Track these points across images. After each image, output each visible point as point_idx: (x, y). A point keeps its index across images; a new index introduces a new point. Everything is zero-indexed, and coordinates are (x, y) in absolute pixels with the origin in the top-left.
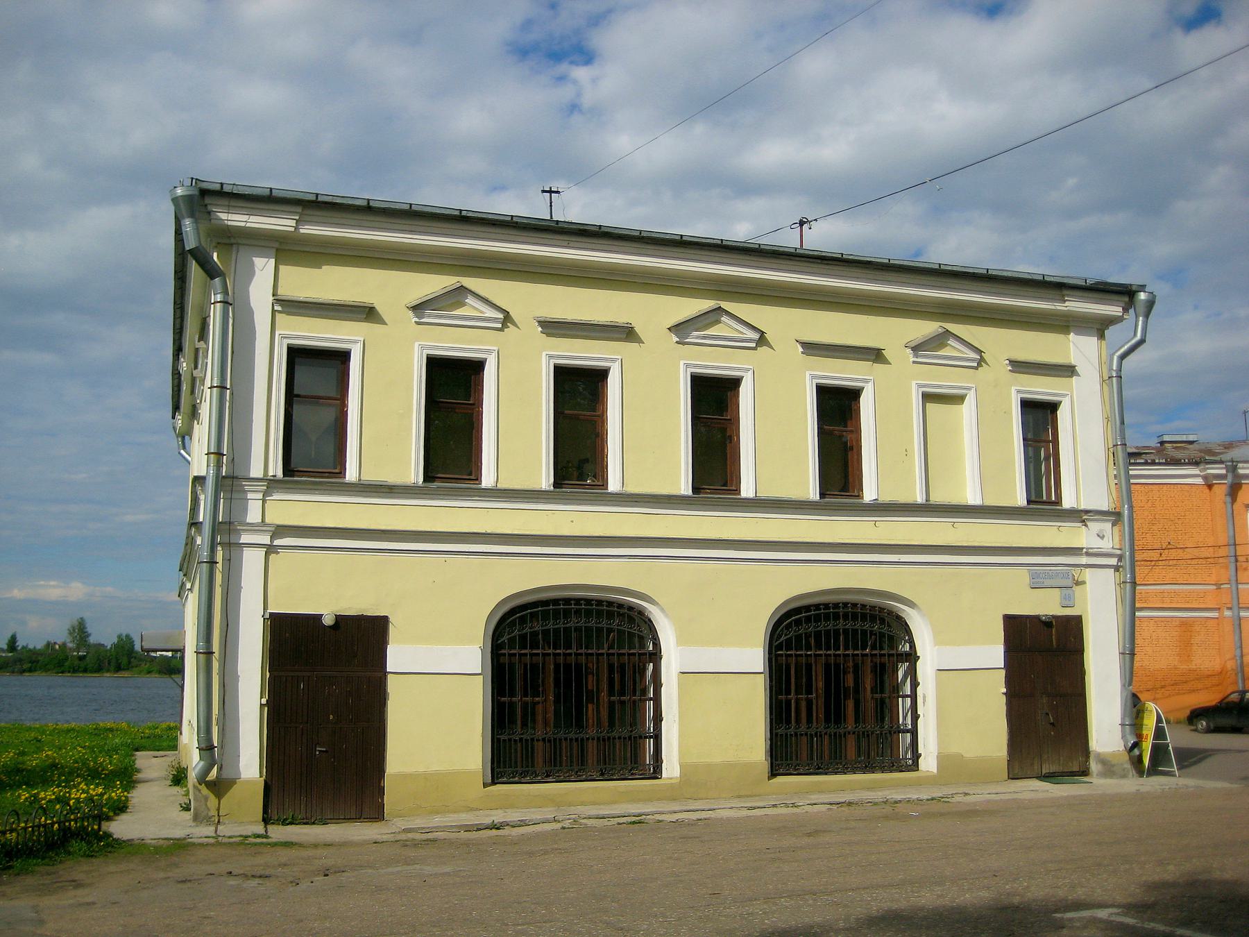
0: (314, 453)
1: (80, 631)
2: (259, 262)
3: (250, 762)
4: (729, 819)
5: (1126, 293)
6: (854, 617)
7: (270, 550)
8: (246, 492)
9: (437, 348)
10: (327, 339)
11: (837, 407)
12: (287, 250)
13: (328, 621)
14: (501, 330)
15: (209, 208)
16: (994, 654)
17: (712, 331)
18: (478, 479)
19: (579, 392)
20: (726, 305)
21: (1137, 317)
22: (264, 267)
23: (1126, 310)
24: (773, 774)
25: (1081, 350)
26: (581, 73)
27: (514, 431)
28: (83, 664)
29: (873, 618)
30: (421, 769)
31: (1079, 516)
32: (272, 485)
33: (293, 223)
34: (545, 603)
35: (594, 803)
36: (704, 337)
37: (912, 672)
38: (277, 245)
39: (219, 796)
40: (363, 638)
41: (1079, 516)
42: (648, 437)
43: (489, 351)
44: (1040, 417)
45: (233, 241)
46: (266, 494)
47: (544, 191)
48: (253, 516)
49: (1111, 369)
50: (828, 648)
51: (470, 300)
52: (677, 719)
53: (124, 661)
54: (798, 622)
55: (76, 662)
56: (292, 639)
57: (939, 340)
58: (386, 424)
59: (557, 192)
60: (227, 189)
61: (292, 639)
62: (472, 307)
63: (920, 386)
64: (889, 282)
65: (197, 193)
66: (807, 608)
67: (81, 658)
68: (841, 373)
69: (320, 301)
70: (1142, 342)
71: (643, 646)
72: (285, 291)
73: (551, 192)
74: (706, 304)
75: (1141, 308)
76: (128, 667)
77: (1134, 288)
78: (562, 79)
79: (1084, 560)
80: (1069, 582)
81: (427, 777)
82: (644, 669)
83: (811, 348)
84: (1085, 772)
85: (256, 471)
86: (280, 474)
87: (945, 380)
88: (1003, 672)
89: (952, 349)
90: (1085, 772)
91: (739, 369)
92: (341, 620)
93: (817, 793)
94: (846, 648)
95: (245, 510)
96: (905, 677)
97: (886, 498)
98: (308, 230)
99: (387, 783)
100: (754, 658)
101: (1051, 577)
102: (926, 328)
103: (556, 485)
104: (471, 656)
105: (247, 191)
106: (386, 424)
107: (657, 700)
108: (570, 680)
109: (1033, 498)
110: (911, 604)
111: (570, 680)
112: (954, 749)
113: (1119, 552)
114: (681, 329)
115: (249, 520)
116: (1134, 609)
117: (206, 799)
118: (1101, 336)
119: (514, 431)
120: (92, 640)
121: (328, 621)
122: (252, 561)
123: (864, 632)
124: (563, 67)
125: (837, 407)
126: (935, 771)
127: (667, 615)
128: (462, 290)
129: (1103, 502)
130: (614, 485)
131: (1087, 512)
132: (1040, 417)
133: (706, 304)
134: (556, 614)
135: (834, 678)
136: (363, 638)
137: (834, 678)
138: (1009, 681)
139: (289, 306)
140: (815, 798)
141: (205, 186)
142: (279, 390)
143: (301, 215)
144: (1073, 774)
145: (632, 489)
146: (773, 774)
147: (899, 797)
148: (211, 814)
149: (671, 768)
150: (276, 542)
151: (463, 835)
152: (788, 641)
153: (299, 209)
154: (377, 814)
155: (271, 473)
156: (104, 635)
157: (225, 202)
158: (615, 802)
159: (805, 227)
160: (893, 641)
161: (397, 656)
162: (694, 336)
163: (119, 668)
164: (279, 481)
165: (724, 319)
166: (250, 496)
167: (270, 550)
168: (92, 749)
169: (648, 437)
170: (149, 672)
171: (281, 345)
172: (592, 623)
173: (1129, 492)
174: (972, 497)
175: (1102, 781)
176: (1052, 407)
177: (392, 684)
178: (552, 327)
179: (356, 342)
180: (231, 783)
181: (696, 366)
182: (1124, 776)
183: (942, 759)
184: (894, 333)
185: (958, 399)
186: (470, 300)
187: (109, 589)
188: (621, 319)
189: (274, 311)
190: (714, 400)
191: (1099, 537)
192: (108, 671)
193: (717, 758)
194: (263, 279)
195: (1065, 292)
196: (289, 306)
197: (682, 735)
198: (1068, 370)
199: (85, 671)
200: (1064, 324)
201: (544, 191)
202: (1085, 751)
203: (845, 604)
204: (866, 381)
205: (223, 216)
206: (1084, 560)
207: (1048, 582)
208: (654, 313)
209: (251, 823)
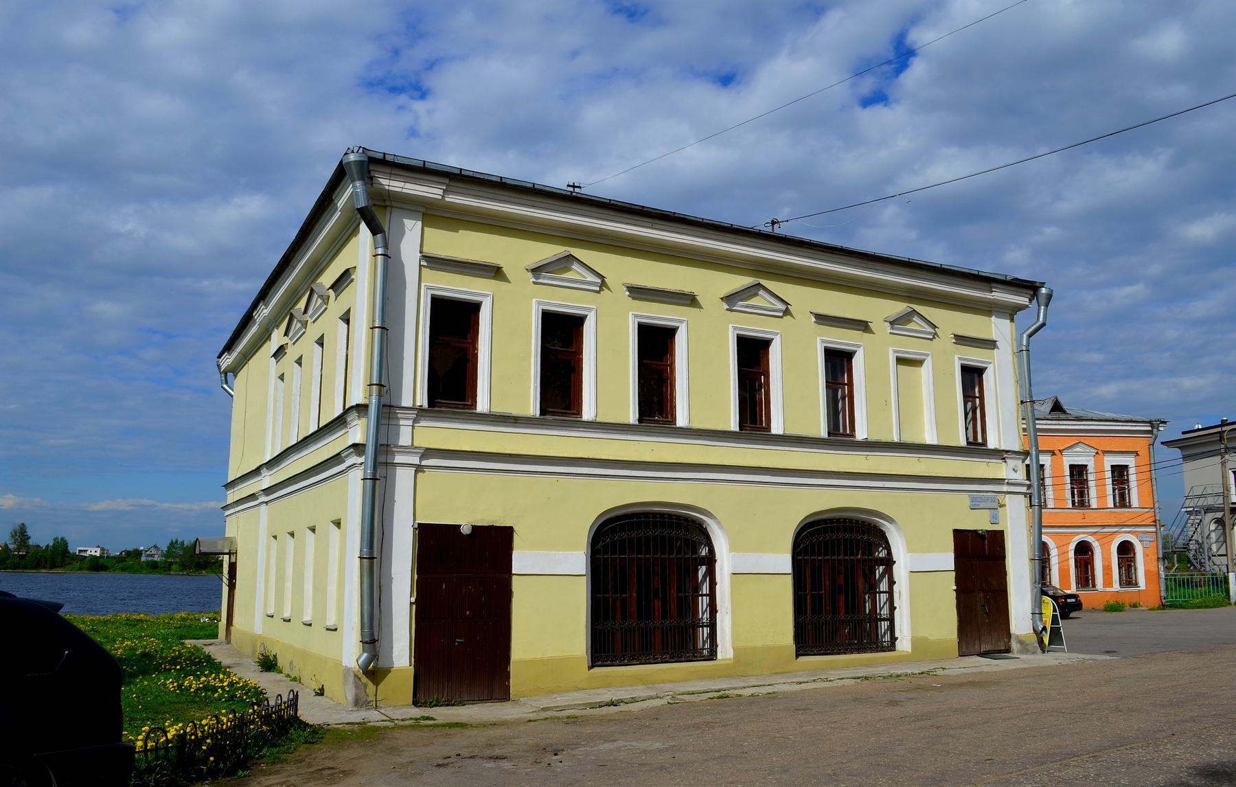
0: (452, 384)
1: (21, 534)
2: (408, 223)
3: (401, 652)
4: (792, 693)
5: (1032, 288)
7: (419, 469)
8: (398, 419)
9: (549, 304)
11: (838, 363)
12: (432, 214)
13: (466, 530)
14: (598, 292)
15: (372, 173)
16: (947, 560)
17: (752, 302)
18: (579, 413)
19: (655, 346)
20: (763, 282)
22: (412, 228)
23: (1030, 301)
24: (797, 656)
25: (999, 328)
26: (419, 106)
27: (608, 379)
28: (23, 562)
29: (679, 527)
30: (539, 656)
31: (1000, 454)
32: (421, 413)
33: (441, 192)
35: (671, 682)
36: (747, 307)
37: (711, 573)
39: (376, 683)
40: (494, 544)
41: (1000, 454)
43: (590, 310)
44: (972, 376)
45: (388, 203)
46: (415, 421)
48: (404, 439)
49: (1021, 345)
50: (663, 552)
51: (575, 266)
52: (729, 611)
53: (59, 560)
54: (812, 534)
55: (17, 560)
56: (435, 542)
58: (507, 367)
60: (388, 158)
61: (435, 542)
62: (576, 272)
63: (895, 351)
64: (876, 270)
66: (825, 521)
67: (22, 557)
70: (1043, 325)
71: (695, 551)
72: (430, 250)
74: (745, 281)
75: (1043, 300)
76: (63, 564)
78: (401, 108)
79: (1005, 488)
80: (995, 505)
81: (544, 662)
82: (697, 571)
83: (822, 319)
84: (1008, 651)
85: (406, 401)
86: (426, 405)
87: (912, 348)
88: (954, 574)
89: (916, 324)
90: (1008, 651)
92: (476, 529)
93: (841, 669)
94: (845, 554)
95: (398, 434)
96: (704, 577)
97: (874, 437)
98: (452, 199)
99: (513, 668)
100: (785, 563)
103: (640, 420)
104: (577, 561)
105: (406, 162)
106: (507, 367)
107: (712, 595)
108: (648, 580)
109: (971, 440)
110: (890, 520)
111: (648, 580)
112: (922, 633)
114: (731, 299)
115: (401, 443)
116: (1041, 527)
117: (365, 686)
118: (1012, 320)
119: (608, 379)
120: (31, 542)
121: (466, 530)
122: (403, 479)
123: (858, 542)
124: (403, 99)
126: (910, 650)
127: (899, 529)
128: (570, 258)
129: (1013, 442)
130: (681, 421)
131: (1007, 452)
132: (972, 376)
135: (838, 574)
136: (494, 544)
137: (838, 574)
139: (433, 262)
140: (843, 674)
141: (370, 154)
142: (424, 332)
143: (448, 185)
144: (1000, 652)
145: (696, 425)
146: (797, 656)
147: (899, 672)
148: (370, 699)
149: (725, 650)
150: (424, 463)
151: (589, 712)
152: (806, 548)
153: (447, 181)
154: (502, 694)
155: (418, 403)
156: (41, 538)
157: (388, 170)
158: (686, 680)
160: (870, 548)
161: (520, 561)
162: (740, 305)
163: (53, 566)
164: (424, 410)
165: (761, 292)
166: (402, 422)
167: (419, 469)
168: (165, 639)
169: (704, 385)
170: (80, 569)
171: (426, 294)
173: (1036, 440)
174: (930, 438)
175: (1023, 657)
176: (979, 372)
177: (516, 582)
178: (638, 292)
179: (487, 296)
180: (387, 671)
181: (741, 329)
182: (1034, 653)
183: (915, 642)
184: (878, 310)
185: (917, 363)
186: (575, 266)
187: (37, 500)
188: (687, 289)
189: (420, 266)
192: (45, 568)
193: (759, 643)
194: (413, 237)
196: (433, 262)
197: (734, 624)
198: (991, 344)
199: (24, 567)
202: (1009, 635)
203: (845, 520)
205: (384, 182)
206: (1005, 488)
207: (982, 505)
208: (713, 285)
209: (403, 706)
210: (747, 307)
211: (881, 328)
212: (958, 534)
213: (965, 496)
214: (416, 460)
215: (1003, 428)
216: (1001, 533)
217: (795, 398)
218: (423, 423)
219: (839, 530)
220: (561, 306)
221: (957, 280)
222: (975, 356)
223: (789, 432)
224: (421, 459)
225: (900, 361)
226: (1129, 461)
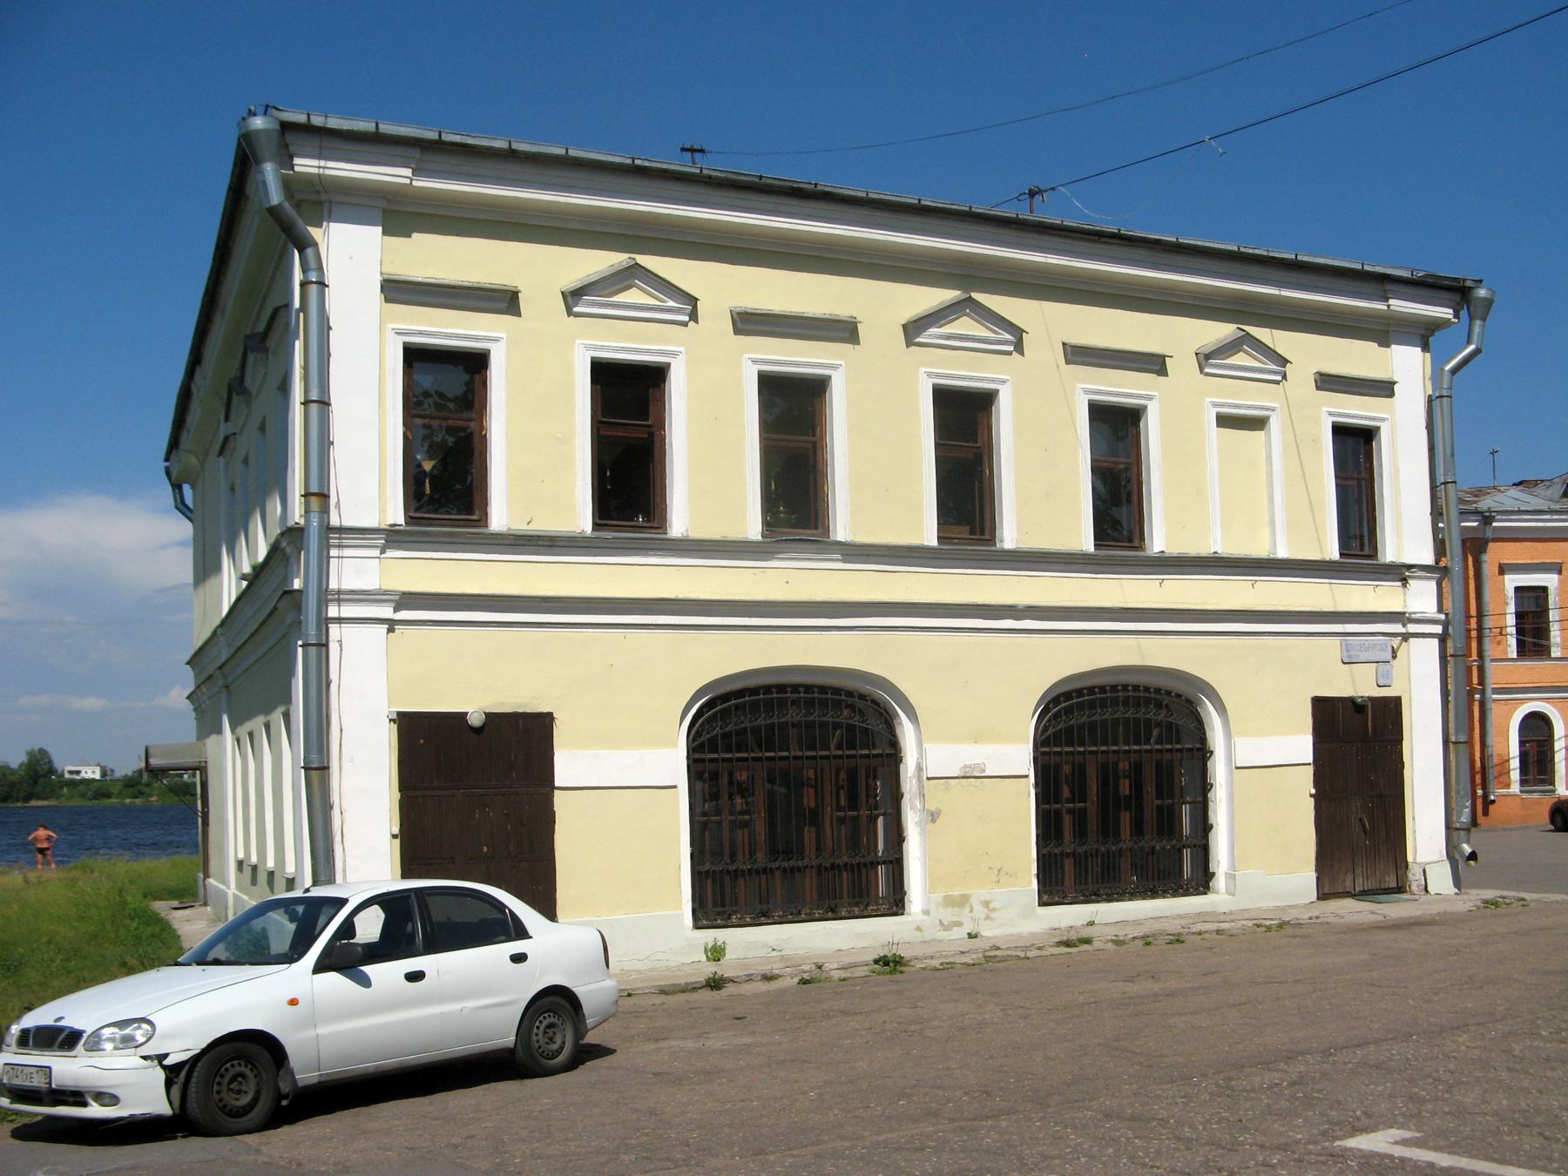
6: (1137, 703)
10: (458, 337)
11: (1117, 428)
12: (398, 214)
13: (476, 720)
14: (685, 324)
15: (292, 149)
16: (1302, 747)
19: (792, 409)
21: (1471, 319)
23: (1456, 316)
25: (1407, 365)
27: (712, 463)
31: (1400, 573)
32: (393, 538)
34: (754, 691)
36: (948, 337)
38: (385, 205)
40: (521, 743)
41: (1400, 573)
42: (881, 472)
44: (1355, 447)
45: (324, 197)
47: (684, 149)
57: (1231, 347)
58: (538, 456)
59: (701, 151)
65: (277, 127)
68: (1121, 387)
69: (446, 282)
73: (692, 150)
74: (948, 295)
77: (1469, 284)
87: (1248, 398)
88: (1311, 769)
91: (993, 381)
92: (491, 717)
98: (422, 183)
100: (1020, 757)
101: (1367, 649)
102: (1219, 331)
106: (538, 456)
113: (1443, 617)
118: (1425, 347)
121: (476, 720)
125: (1117, 428)
132: (1355, 447)
133: (948, 295)
134: (770, 705)
135: (1119, 780)
136: (521, 743)
137: (1119, 780)
138: (1318, 781)
153: (416, 153)
157: (315, 141)
159: (1038, 198)
161: (568, 766)
169: (881, 472)
172: (815, 717)
177: (560, 801)
178: (748, 323)
190: (963, 419)
191: (1422, 598)
195: (1389, 287)
196: (397, 290)
198: (1384, 388)
200: (1384, 332)
201: (684, 149)
204: (1150, 398)
208: (885, 304)
210: (948, 337)
211: (1182, 366)
212: (1322, 706)
213: (1337, 641)
214: (387, 612)
215: (1406, 530)
216: (1397, 701)
217: (1042, 491)
218: (390, 553)
219: (1115, 702)
220: (623, 350)
221: (1327, 281)
222: (1357, 410)
223: (385, 587)
224: (396, 610)
225: (1224, 421)
226: (1549, 580)
